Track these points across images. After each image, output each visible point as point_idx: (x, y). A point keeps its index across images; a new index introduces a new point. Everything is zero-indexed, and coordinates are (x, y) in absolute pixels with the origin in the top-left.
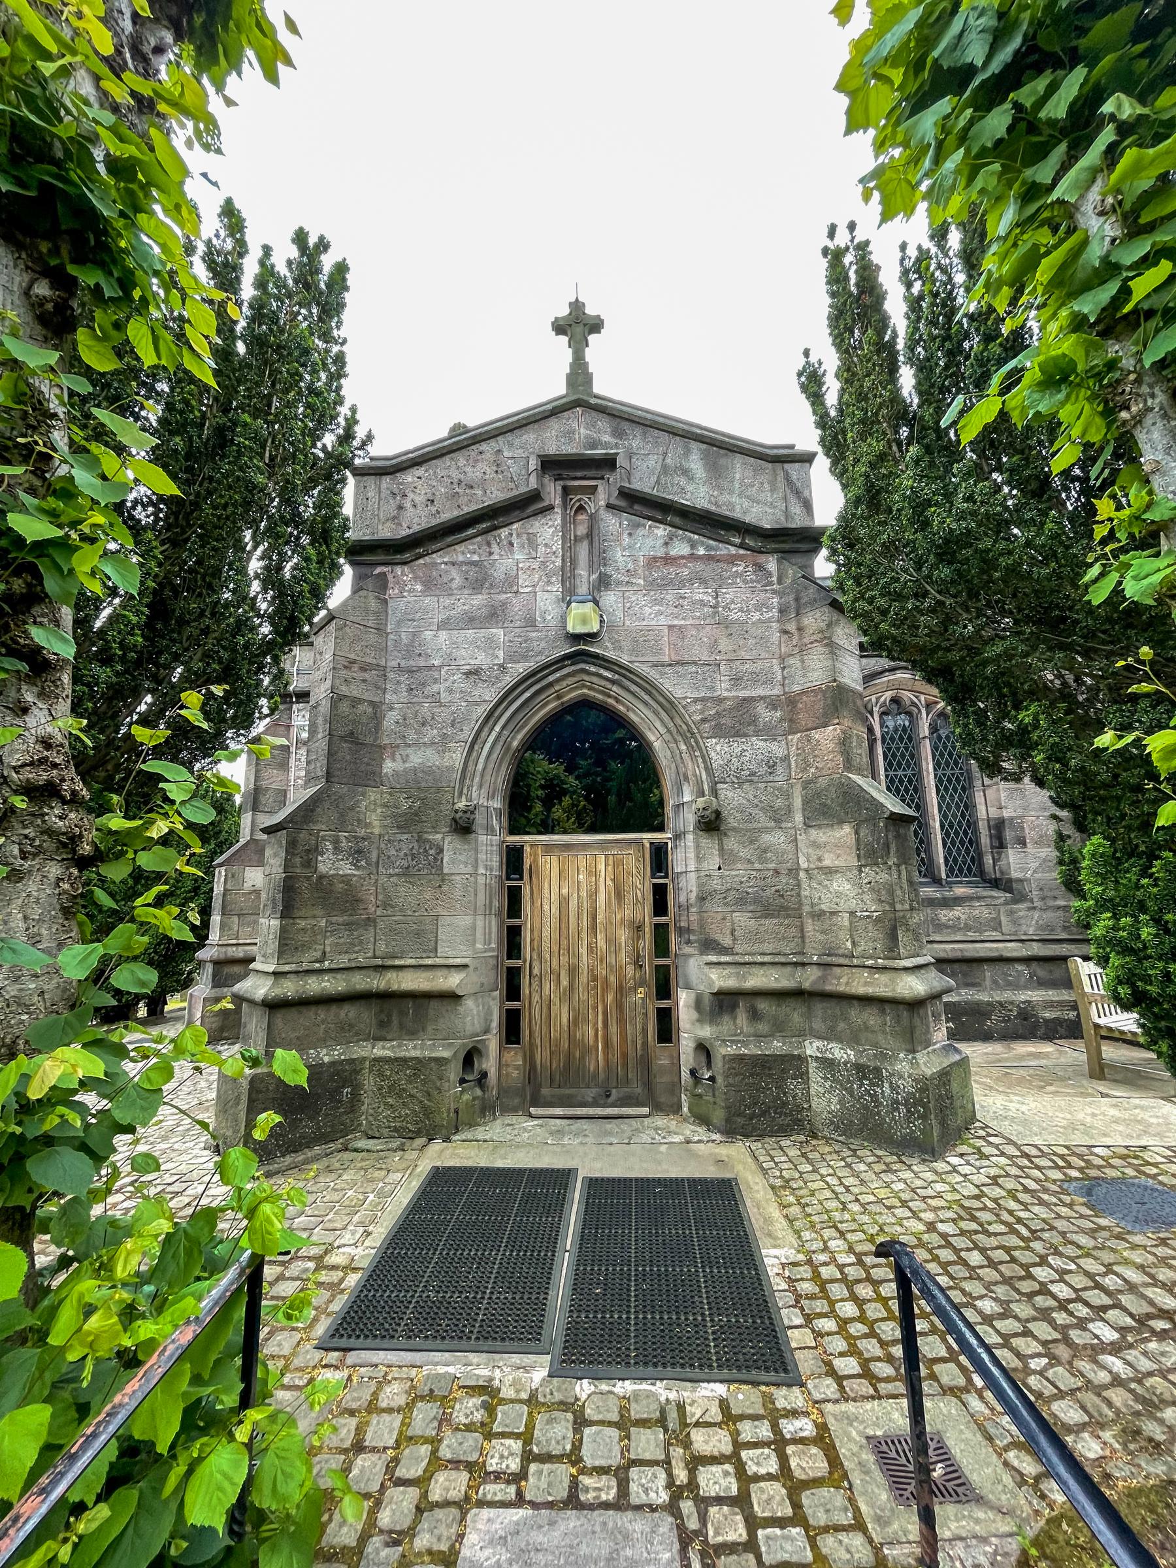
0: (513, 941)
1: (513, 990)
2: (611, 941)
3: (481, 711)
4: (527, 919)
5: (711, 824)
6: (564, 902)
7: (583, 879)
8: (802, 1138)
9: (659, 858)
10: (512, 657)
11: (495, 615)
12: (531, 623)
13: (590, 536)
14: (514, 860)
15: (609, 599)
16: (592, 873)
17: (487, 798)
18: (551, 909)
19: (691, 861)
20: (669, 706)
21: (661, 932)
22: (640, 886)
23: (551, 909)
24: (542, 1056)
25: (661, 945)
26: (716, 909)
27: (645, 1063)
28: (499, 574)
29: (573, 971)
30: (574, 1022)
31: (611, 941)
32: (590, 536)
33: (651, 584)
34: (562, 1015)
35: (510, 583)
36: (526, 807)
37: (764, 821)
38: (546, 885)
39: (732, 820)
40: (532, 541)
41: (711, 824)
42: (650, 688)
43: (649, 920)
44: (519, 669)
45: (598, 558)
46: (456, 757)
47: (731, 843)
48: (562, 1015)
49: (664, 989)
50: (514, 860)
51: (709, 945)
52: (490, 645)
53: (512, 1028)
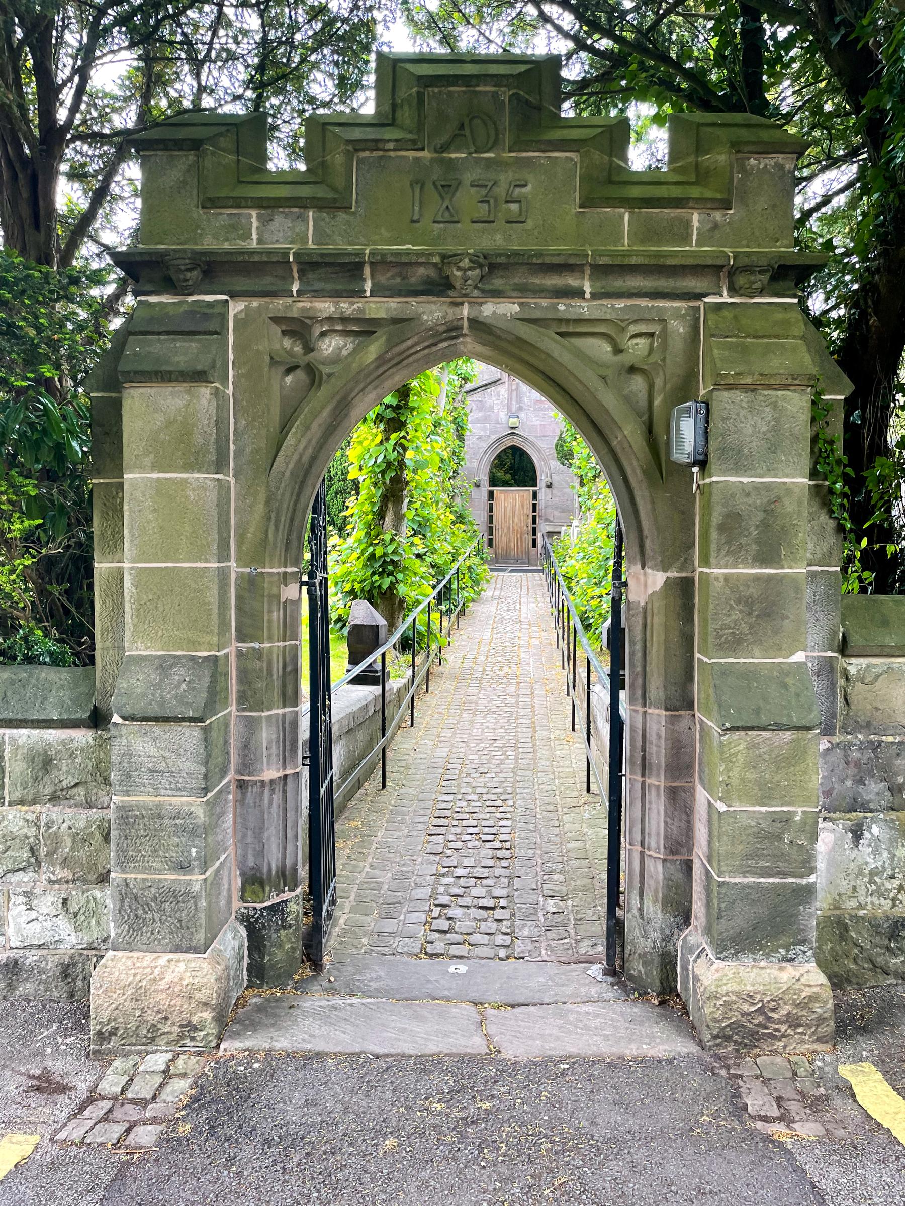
0: (491, 517)
1: (491, 533)
2: (520, 520)
3: (482, 451)
4: (494, 513)
5: (549, 486)
6: (506, 508)
7: (513, 499)
8: (862, 913)
9: (535, 495)
10: (491, 433)
11: (486, 419)
12: (497, 422)
13: (517, 390)
14: (491, 494)
15: (522, 415)
16: (515, 499)
17: (484, 478)
18: (502, 510)
19: (544, 495)
20: (539, 451)
21: (534, 517)
22: (529, 503)
23: (502, 510)
24: (499, 551)
25: (534, 522)
26: (549, 510)
27: (528, 552)
28: (487, 405)
29: (508, 528)
30: (509, 542)
31: (520, 520)
32: (517, 390)
33: (535, 410)
34: (505, 539)
35: (491, 408)
36: (494, 482)
37: (565, 485)
38: (623, 809)
39: (555, 485)
40: (498, 394)
41: (549, 486)
42: (533, 444)
43: (531, 514)
44: (494, 437)
45: (519, 400)
46: (475, 464)
47: (555, 491)
48: (505, 539)
49: (534, 534)
50: (491, 494)
51: (547, 520)
52: (484, 429)
53: (490, 543)
